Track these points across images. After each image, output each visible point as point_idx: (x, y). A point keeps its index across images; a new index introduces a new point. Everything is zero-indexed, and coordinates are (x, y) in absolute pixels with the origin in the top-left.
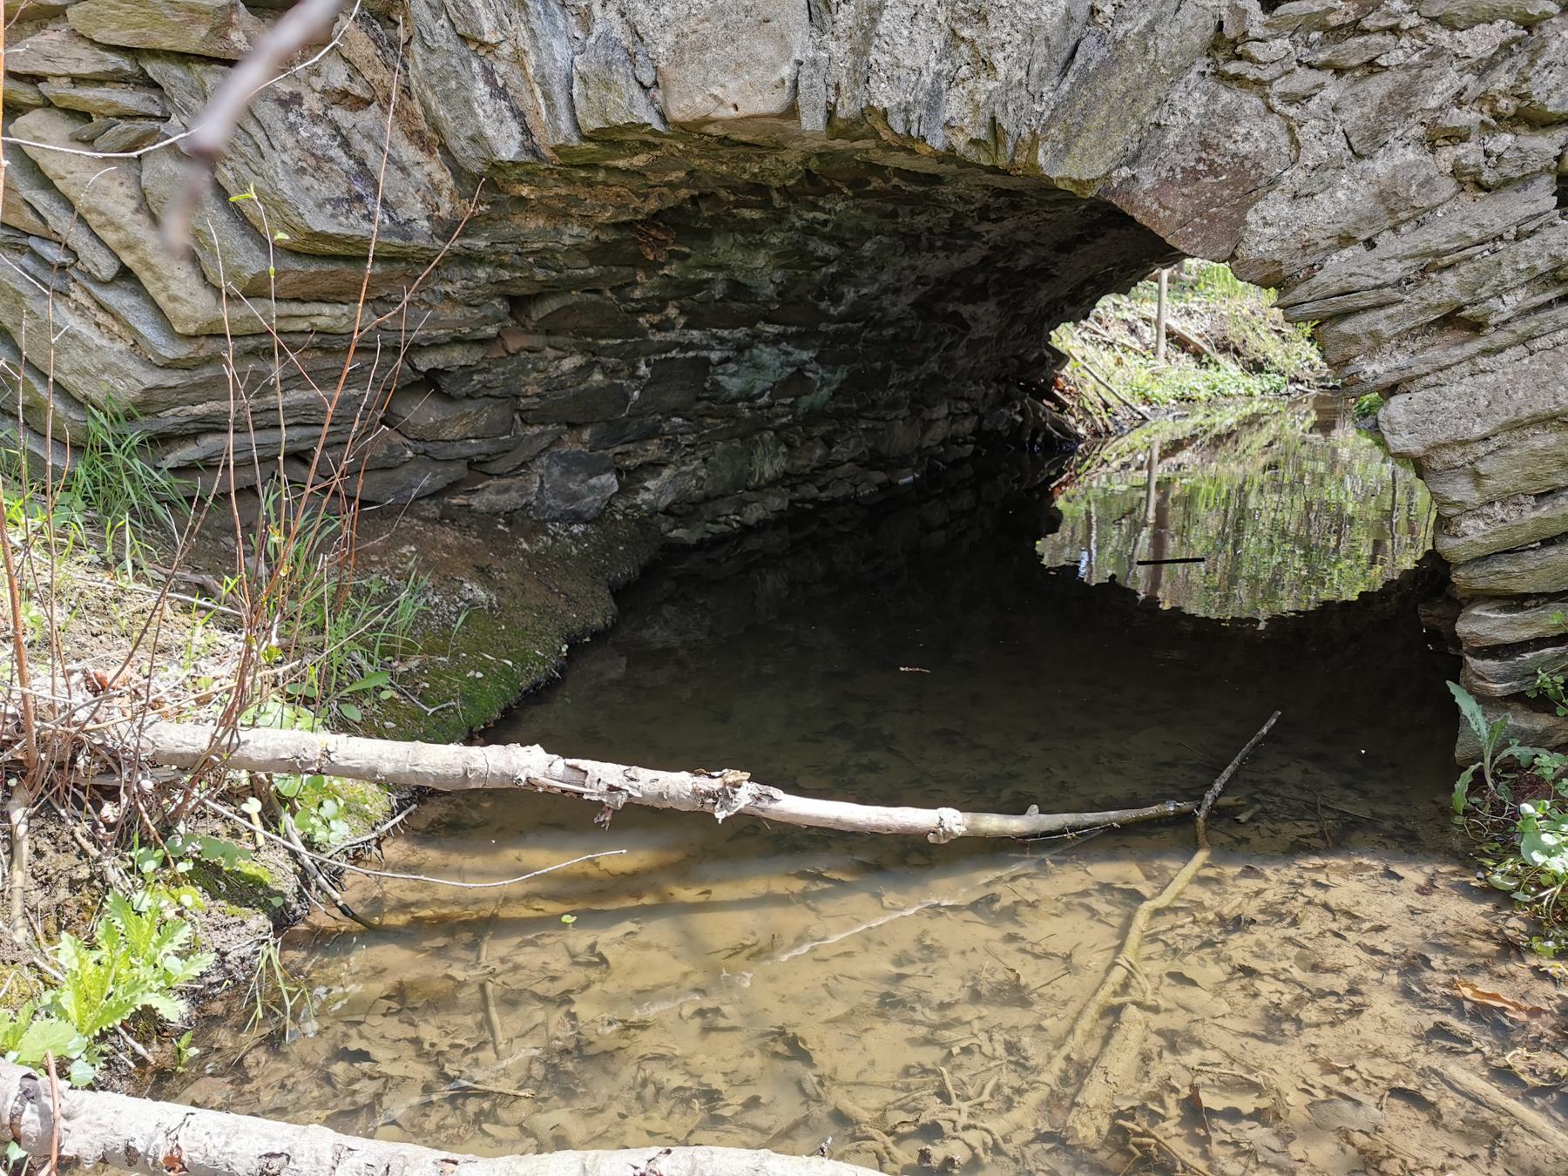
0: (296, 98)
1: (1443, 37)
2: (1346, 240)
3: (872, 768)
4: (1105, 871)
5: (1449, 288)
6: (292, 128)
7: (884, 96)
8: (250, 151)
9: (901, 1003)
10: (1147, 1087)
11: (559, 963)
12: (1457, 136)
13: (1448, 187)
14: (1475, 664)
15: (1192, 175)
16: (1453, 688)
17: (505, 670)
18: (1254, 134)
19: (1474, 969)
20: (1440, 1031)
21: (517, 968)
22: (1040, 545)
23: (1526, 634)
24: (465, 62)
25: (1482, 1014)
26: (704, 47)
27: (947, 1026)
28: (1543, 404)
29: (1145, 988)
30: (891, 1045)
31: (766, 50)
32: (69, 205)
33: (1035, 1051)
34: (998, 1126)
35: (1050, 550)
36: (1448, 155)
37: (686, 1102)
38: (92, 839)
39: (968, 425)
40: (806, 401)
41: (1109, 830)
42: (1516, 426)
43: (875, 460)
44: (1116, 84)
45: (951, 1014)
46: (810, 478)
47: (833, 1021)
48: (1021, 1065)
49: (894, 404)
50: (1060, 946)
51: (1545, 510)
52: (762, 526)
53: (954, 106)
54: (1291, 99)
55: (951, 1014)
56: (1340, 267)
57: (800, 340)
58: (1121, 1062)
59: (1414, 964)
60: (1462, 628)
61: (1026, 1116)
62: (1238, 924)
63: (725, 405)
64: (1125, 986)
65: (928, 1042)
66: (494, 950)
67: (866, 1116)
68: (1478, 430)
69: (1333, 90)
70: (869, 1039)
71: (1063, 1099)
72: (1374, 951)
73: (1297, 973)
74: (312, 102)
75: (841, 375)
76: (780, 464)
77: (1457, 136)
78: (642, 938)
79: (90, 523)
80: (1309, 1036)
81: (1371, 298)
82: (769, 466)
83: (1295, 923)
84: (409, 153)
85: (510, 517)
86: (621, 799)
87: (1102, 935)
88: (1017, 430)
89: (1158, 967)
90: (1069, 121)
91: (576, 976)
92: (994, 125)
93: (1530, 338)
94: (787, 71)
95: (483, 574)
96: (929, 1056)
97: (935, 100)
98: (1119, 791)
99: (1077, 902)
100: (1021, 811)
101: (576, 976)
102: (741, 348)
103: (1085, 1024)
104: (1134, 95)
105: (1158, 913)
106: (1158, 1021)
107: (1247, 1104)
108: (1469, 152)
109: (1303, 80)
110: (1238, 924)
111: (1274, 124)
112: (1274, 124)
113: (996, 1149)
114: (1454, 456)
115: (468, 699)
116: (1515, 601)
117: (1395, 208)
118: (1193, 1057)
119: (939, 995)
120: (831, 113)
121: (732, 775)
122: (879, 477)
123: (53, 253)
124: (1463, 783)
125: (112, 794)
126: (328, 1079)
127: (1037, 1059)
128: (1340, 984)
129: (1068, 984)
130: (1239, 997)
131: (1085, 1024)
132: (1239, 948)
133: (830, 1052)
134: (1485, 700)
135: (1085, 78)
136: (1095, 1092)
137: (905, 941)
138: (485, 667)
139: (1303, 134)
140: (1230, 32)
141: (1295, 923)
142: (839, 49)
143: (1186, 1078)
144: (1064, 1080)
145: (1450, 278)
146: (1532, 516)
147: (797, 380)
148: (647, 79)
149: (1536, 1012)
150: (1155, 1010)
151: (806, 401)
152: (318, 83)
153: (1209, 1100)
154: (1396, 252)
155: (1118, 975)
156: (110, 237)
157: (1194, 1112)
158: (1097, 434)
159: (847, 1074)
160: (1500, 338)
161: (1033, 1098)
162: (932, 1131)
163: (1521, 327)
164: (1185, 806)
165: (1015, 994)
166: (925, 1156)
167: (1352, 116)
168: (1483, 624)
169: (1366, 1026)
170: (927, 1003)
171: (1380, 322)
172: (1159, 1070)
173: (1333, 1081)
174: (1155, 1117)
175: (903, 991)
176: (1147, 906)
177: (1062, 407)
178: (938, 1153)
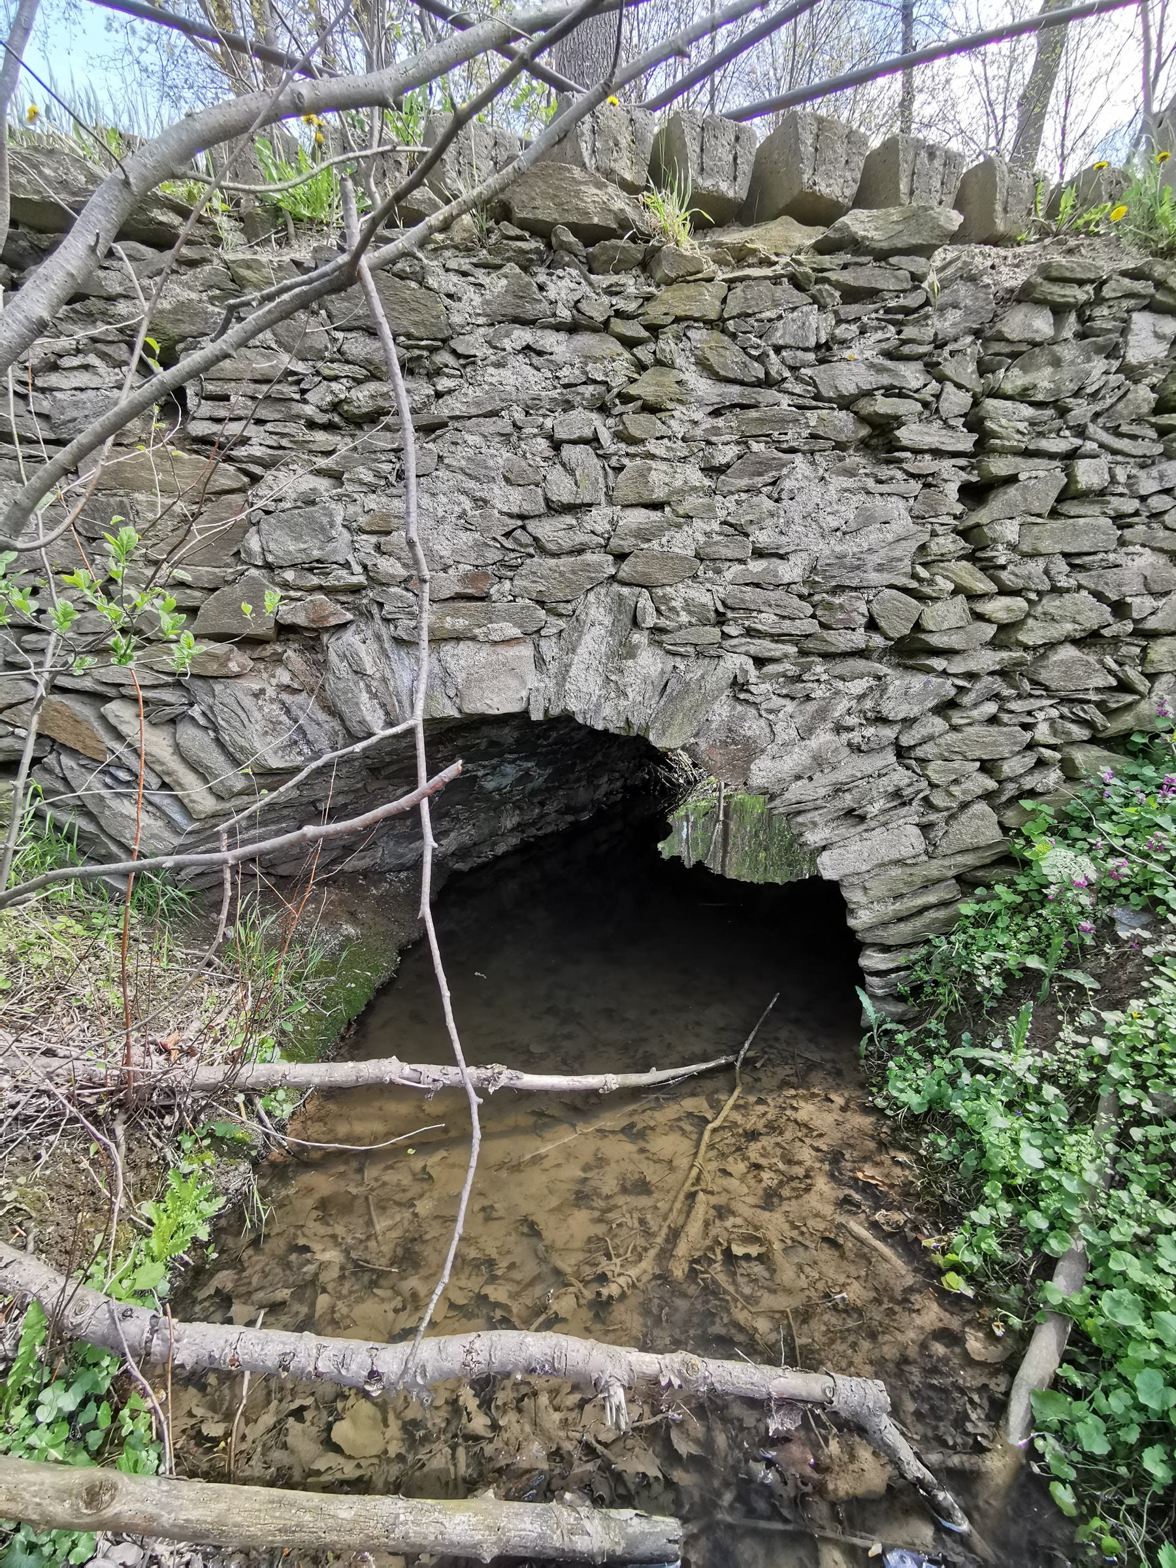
0: (263, 691)
1: (840, 684)
2: (798, 777)
3: (569, 1037)
4: (689, 1104)
5: (848, 800)
6: (260, 708)
7: (574, 706)
8: (238, 725)
9: (587, 1197)
10: (708, 1242)
11: (406, 1180)
12: (850, 729)
13: (847, 751)
14: (869, 979)
15: (725, 744)
16: (859, 991)
17: (367, 979)
18: (753, 727)
19: (865, 1159)
20: (847, 1200)
21: (384, 1184)
22: (660, 846)
23: (891, 965)
24: (356, 683)
25: (866, 1188)
26: (481, 680)
27: (609, 1210)
28: (895, 855)
29: (708, 1181)
30: (581, 1224)
31: (514, 683)
32: (136, 752)
33: (653, 1224)
34: (634, 1272)
35: (665, 848)
36: (845, 736)
37: (478, 1267)
38: (158, 1137)
39: (619, 784)
40: (530, 786)
41: (692, 1077)
42: (883, 865)
43: (568, 810)
44: (687, 703)
45: (612, 1202)
46: (534, 824)
47: (552, 1210)
48: (648, 1234)
49: (578, 780)
50: (666, 1154)
51: (898, 906)
52: (506, 855)
53: (607, 710)
54: (770, 711)
55: (612, 1202)
56: (797, 790)
57: (527, 759)
58: (694, 1228)
59: (836, 1157)
60: (863, 962)
61: (647, 1265)
62: (753, 1135)
63: (487, 796)
64: (698, 1179)
65: (600, 1220)
66: (372, 1172)
67: (569, 1270)
68: (864, 868)
69: (790, 707)
70: (570, 1220)
71: (666, 1254)
72: (818, 1150)
73: (781, 1166)
74: (271, 692)
75: (549, 771)
76: (516, 820)
77: (850, 729)
78: (450, 1161)
79: (144, 923)
80: (786, 1206)
81: (811, 805)
82: (509, 822)
83: (781, 1133)
84: (322, 716)
85: (365, 873)
86: (440, 1085)
87: (686, 1145)
88: (646, 783)
89: (713, 1166)
90: (665, 718)
91: (416, 1189)
92: (627, 720)
93: (885, 824)
94: (524, 694)
95: (353, 917)
96: (600, 1229)
97: (598, 706)
98: (697, 1049)
99: (674, 1126)
100: (646, 1070)
101: (416, 1189)
102: (494, 768)
103: (678, 1205)
104: (695, 709)
105: (715, 1130)
106: (714, 1200)
107: (754, 1250)
108: (855, 736)
109: (777, 702)
110: (753, 1135)
111: (763, 723)
112: (763, 723)
113: (634, 1286)
114: (855, 880)
115: (348, 1002)
116: (886, 949)
117: (819, 762)
118: (730, 1222)
119: (606, 1190)
120: (546, 711)
121: (498, 1068)
122: (570, 818)
123: (123, 775)
124: (864, 1041)
125: (169, 1109)
126: (288, 1265)
127: (655, 1228)
128: (799, 1171)
129: (672, 1179)
130: (752, 1182)
131: (678, 1205)
132: (754, 1151)
133: (553, 1232)
134: (872, 997)
135: (672, 699)
136: (682, 1249)
137: (587, 1156)
138: (355, 979)
139: (777, 729)
140: (740, 680)
141: (781, 1133)
142: (551, 684)
143: (725, 1235)
144: (667, 1240)
145: (848, 796)
146: (892, 908)
147: (526, 777)
148: (452, 693)
149: (892, 1186)
150: (712, 1193)
151: (530, 786)
152: (274, 682)
153: (738, 1250)
154: (820, 787)
155: (695, 1171)
156: (158, 768)
157: (730, 1258)
158: (689, 782)
159: (559, 1244)
160: (873, 824)
161: (652, 1253)
162: (603, 1278)
163: (882, 819)
164: (731, 1058)
165: (643, 1187)
166: (599, 1294)
167: (799, 720)
168: (871, 960)
169: (812, 1200)
170: (599, 1195)
171: (815, 816)
172: (713, 1231)
173: (795, 1234)
174: (711, 1262)
175: (587, 1189)
176: (710, 1126)
177: (671, 769)
178: (605, 1292)
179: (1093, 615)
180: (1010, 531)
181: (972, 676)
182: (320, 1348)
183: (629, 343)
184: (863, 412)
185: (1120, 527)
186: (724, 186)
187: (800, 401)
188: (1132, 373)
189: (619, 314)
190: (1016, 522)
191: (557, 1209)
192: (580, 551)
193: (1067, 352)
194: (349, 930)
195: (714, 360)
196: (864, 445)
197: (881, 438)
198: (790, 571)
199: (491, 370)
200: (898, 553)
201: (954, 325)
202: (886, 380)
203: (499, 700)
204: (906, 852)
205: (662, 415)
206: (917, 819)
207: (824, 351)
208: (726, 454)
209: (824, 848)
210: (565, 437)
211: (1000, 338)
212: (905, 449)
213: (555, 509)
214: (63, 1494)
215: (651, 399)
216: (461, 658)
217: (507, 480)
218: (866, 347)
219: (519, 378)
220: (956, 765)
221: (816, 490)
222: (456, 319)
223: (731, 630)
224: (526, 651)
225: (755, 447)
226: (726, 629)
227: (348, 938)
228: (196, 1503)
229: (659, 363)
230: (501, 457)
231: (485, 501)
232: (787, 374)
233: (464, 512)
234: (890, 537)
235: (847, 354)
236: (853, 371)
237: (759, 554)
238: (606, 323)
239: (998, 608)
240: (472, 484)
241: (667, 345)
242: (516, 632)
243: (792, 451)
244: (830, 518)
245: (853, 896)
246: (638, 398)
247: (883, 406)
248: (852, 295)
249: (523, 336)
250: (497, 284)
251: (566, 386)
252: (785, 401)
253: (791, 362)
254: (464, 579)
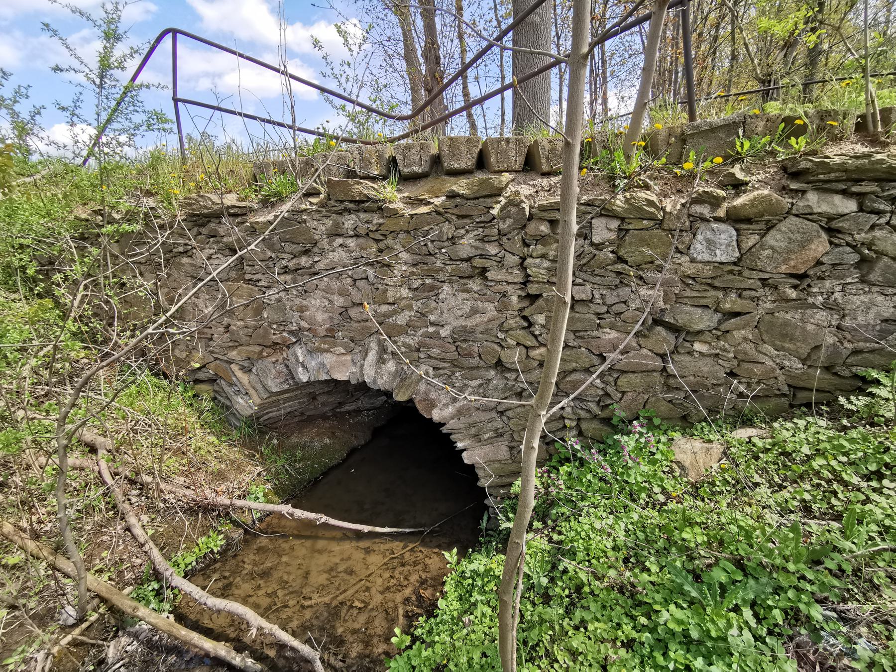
72: (420, 577)
104: (410, 385)
121: (321, 515)
179: (587, 360)
185: (599, 319)
186: (416, 169)
188: (599, 246)
190: (544, 315)
191: (319, 571)
194: (327, 441)
200: (490, 327)
201: (509, 226)
202: (479, 252)
203: (340, 376)
204: (500, 457)
206: (507, 443)
207: (453, 240)
209: (465, 450)
214: (130, 607)
216: (328, 359)
218: (471, 238)
219: (339, 255)
222: (316, 237)
223: (422, 356)
224: (349, 358)
225: (427, 281)
226: (420, 355)
227: (326, 444)
228: (154, 618)
232: (437, 251)
234: (486, 320)
235: (462, 241)
238: (367, 234)
241: (390, 241)
242: (343, 351)
244: (458, 311)
245: (480, 473)
249: (340, 241)
250: (329, 223)
254: (327, 330)
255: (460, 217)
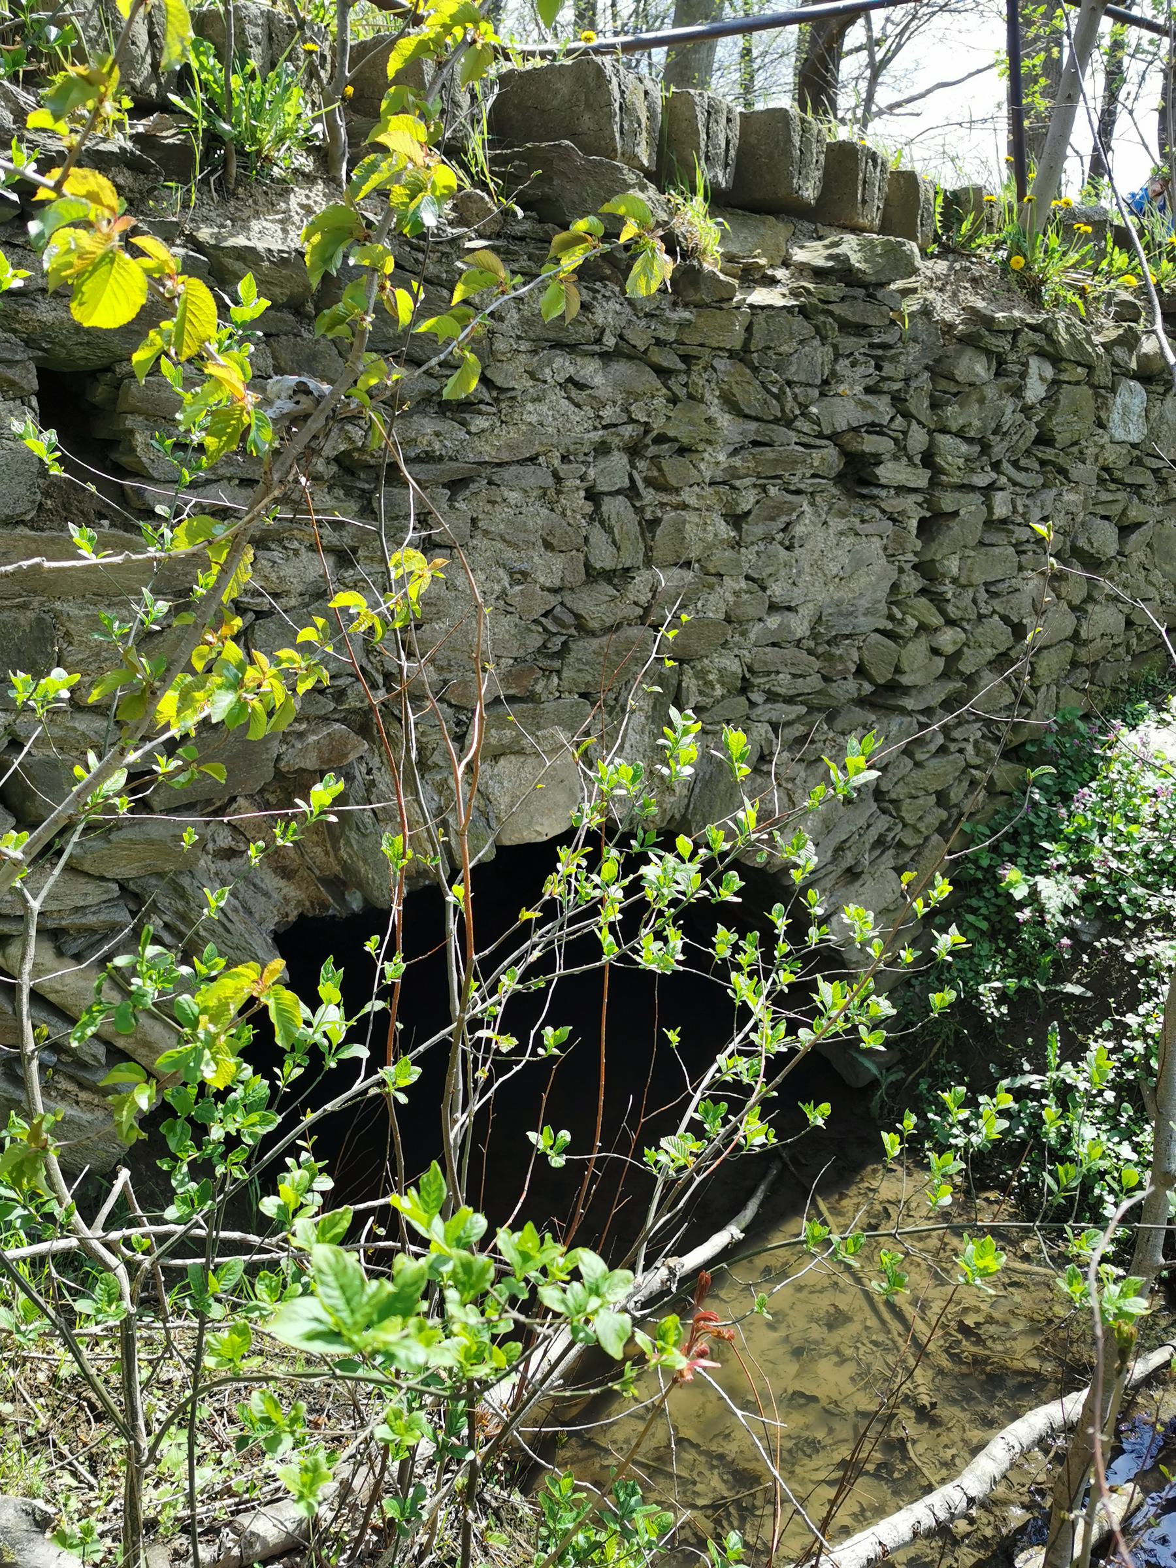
180: (953, 565)
181: (928, 711)
182: (931, 1508)
183: (663, 373)
184: (849, 448)
187: (805, 440)
189: (659, 342)
192: (616, 627)
193: (990, 392)
195: (739, 396)
196: (839, 479)
197: (857, 475)
198: (799, 626)
199: (530, 407)
202: (869, 417)
205: (694, 456)
208: (748, 500)
210: (606, 489)
211: (951, 378)
212: (883, 486)
213: (593, 575)
215: (685, 441)
217: (548, 546)
220: (921, 801)
221: (821, 535)
229: (690, 396)
230: (538, 517)
231: (525, 574)
233: (504, 592)
236: (845, 409)
237: (773, 608)
239: (948, 639)
240: (509, 554)
243: (798, 492)
246: (675, 440)
247: (870, 444)
248: (846, 326)
249: (563, 365)
251: (605, 427)
252: (793, 437)
253: (801, 399)
255: (846, 326)
